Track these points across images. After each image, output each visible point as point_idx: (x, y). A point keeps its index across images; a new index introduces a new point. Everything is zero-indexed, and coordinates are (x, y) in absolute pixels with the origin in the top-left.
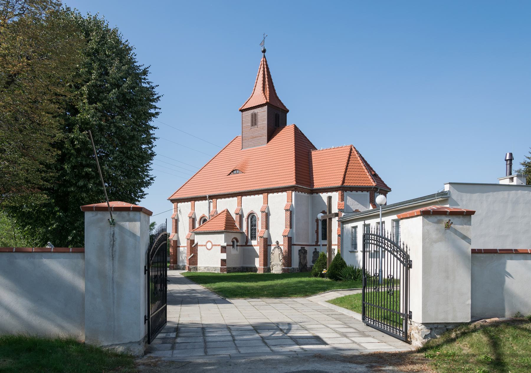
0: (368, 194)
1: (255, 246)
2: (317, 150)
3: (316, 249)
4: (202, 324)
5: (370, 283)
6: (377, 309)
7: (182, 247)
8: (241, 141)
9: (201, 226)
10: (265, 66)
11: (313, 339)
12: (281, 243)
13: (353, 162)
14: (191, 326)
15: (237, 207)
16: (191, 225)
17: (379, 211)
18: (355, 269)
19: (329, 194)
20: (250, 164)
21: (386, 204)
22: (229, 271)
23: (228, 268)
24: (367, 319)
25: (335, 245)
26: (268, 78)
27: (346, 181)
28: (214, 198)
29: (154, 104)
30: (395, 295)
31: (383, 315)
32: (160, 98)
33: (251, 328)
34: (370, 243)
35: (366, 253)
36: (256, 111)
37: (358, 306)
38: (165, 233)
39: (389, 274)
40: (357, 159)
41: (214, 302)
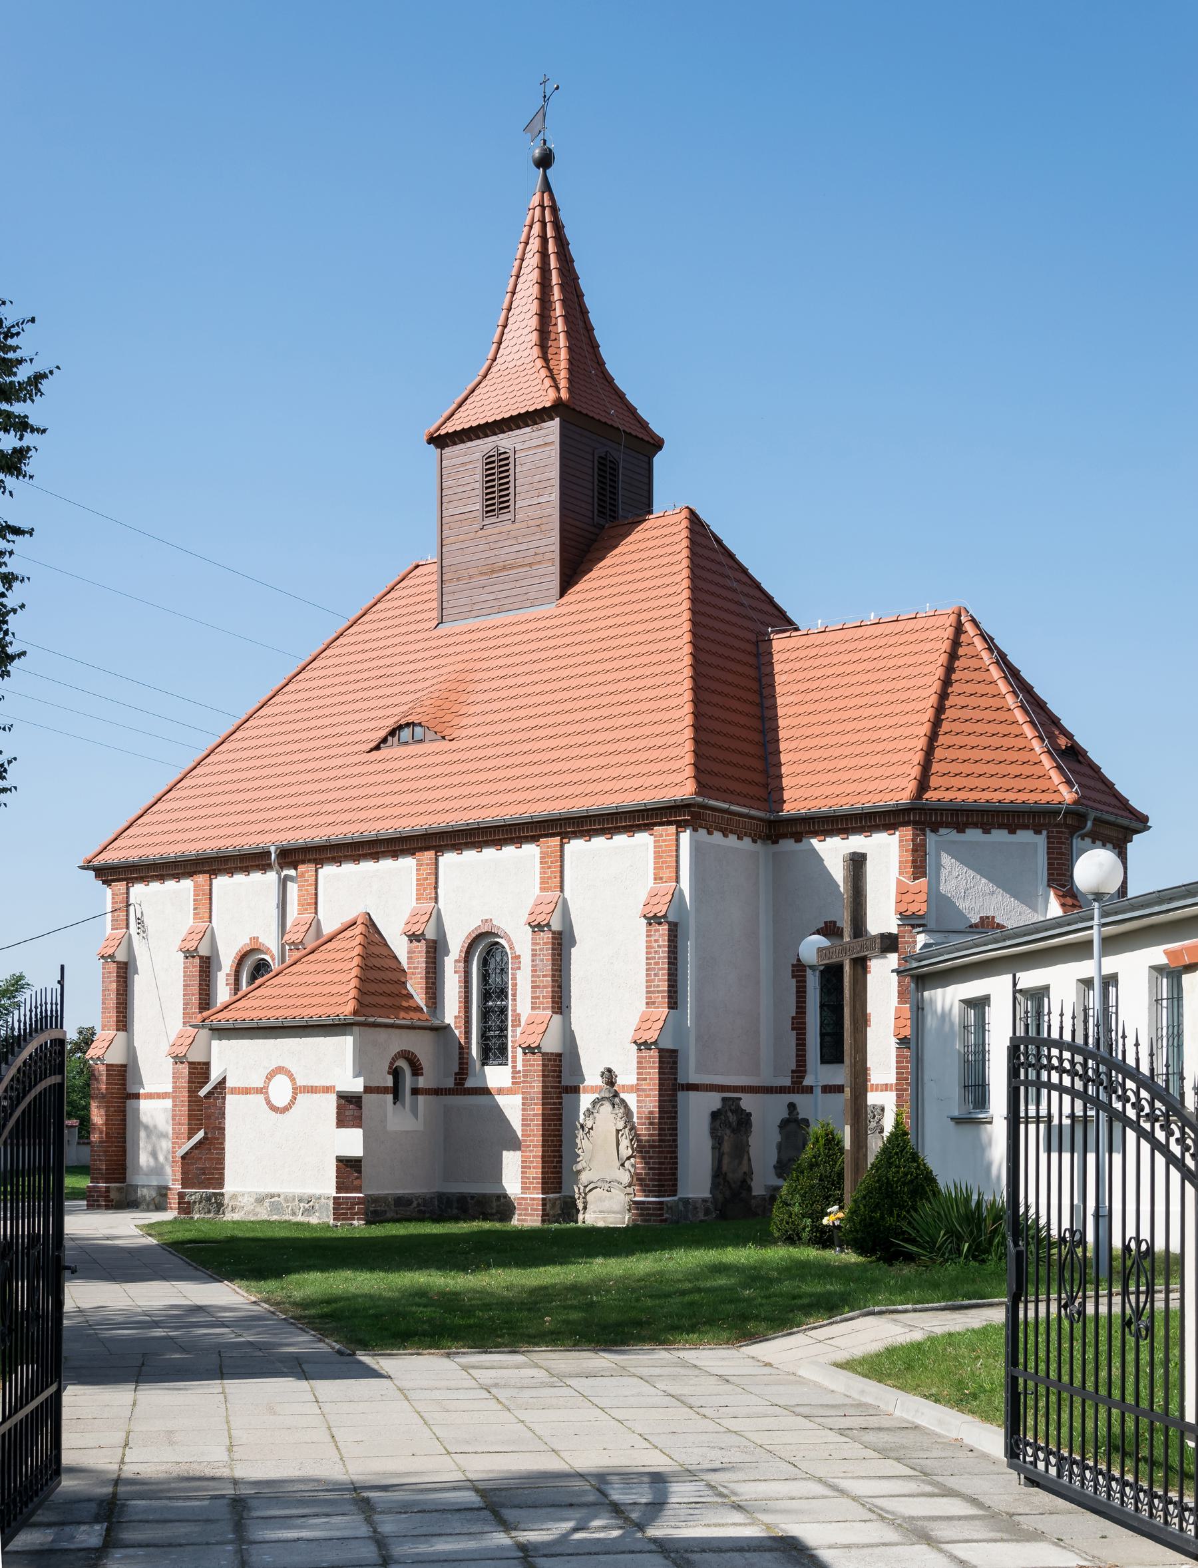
0: (1041, 841)
1: (500, 1091)
2: (797, 629)
3: (792, 1107)
4: (235, 1482)
5: (1043, 1271)
6: (1077, 1401)
7: (150, 1096)
8: (435, 586)
9: (240, 994)
10: (550, 232)
11: (768, 1555)
12: (627, 1077)
13: (969, 688)
14: (180, 1490)
15: (414, 903)
16: (196, 982)
17: (1091, 928)
18: (979, 1203)
19: (857, 843)
20: (479, 697)
21: (1123, 890)
22: (375, 1212)
23: (370, 1200)
24: (1030, 1451)
25: (886, 1087)
26: (562, 286)
27: (934, 781)
28: (303, 862)
29: (17, 408)
30: (1160, 1332)
31: (1103, 1430)
32: (45, 385)
33: (470, 1497)
34: (1039, 1085)
35: (1022, 1127)
36: (504, 441)
37: (988, 1387)
38: (55, 1034)
39: (1131, 1232)
40: (984, 676)
41: (301, 1368)
